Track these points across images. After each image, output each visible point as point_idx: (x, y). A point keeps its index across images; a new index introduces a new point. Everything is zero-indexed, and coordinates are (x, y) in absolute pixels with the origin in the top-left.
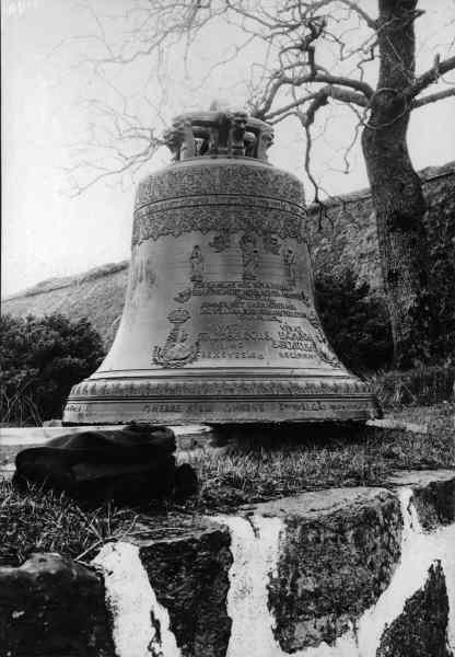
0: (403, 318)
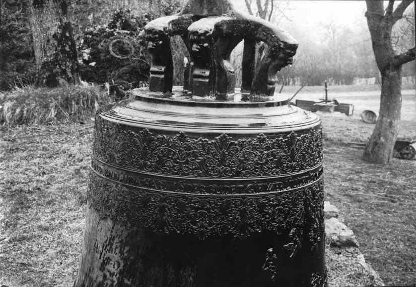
0: (48, 41)
